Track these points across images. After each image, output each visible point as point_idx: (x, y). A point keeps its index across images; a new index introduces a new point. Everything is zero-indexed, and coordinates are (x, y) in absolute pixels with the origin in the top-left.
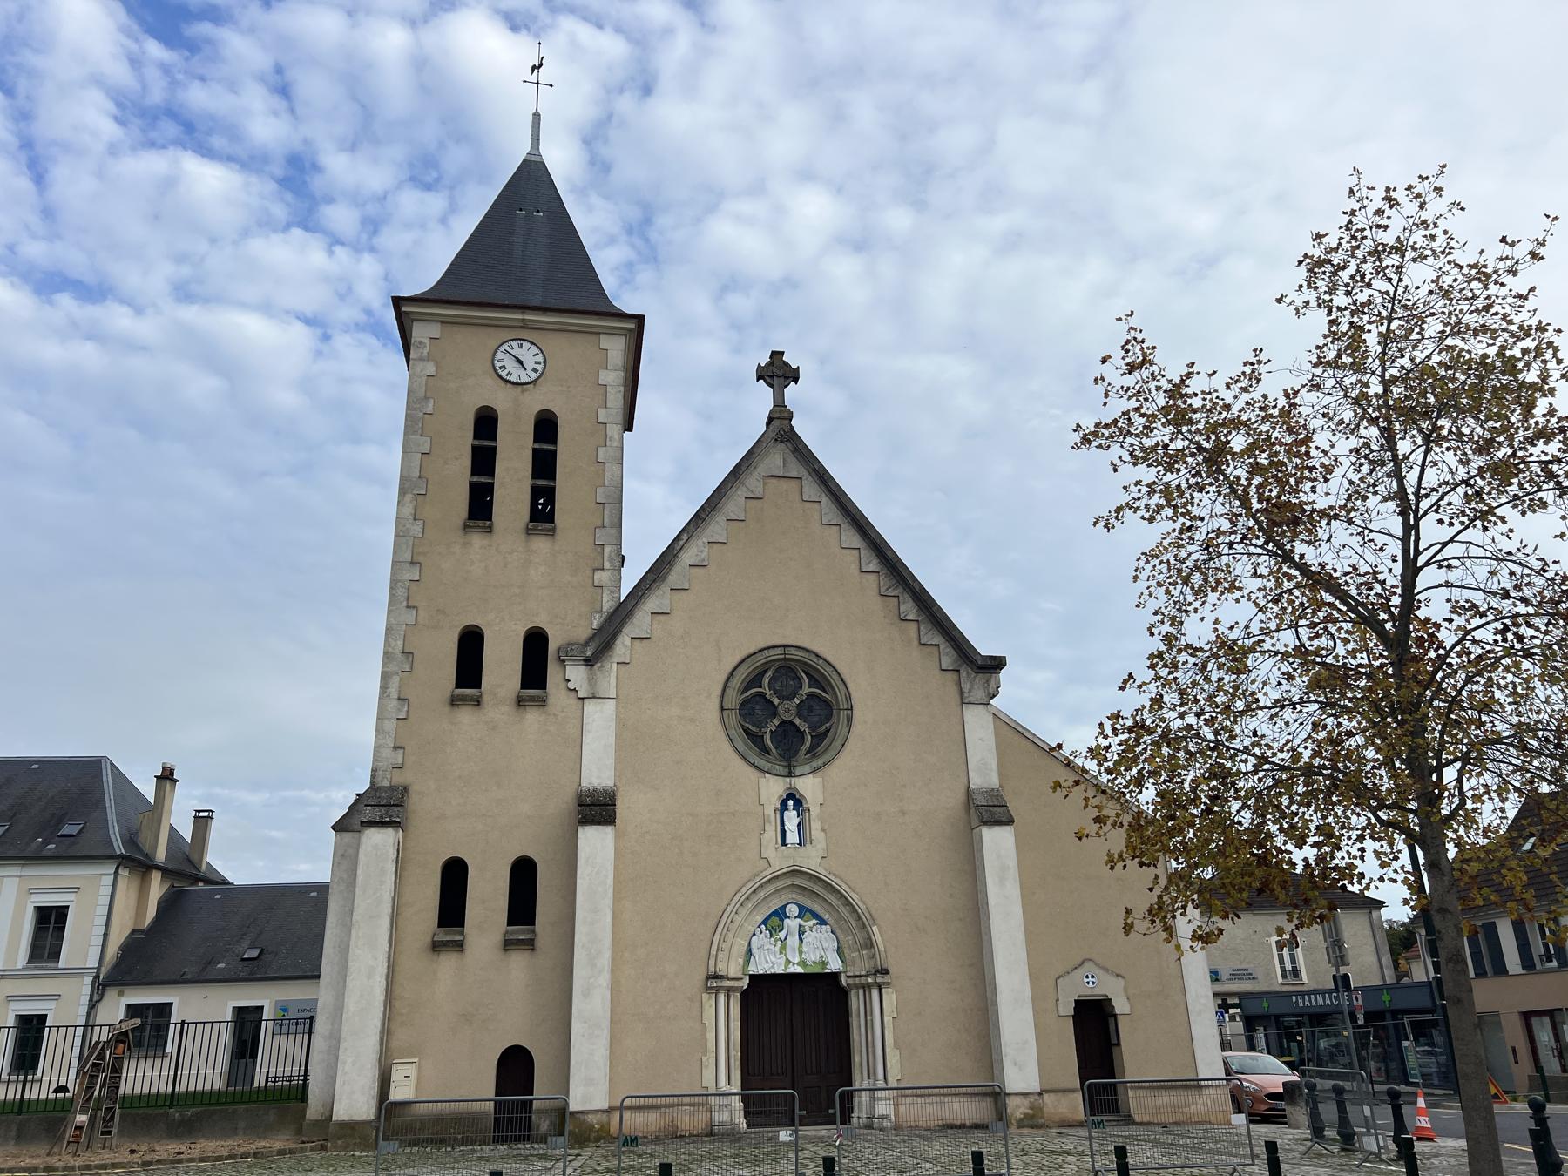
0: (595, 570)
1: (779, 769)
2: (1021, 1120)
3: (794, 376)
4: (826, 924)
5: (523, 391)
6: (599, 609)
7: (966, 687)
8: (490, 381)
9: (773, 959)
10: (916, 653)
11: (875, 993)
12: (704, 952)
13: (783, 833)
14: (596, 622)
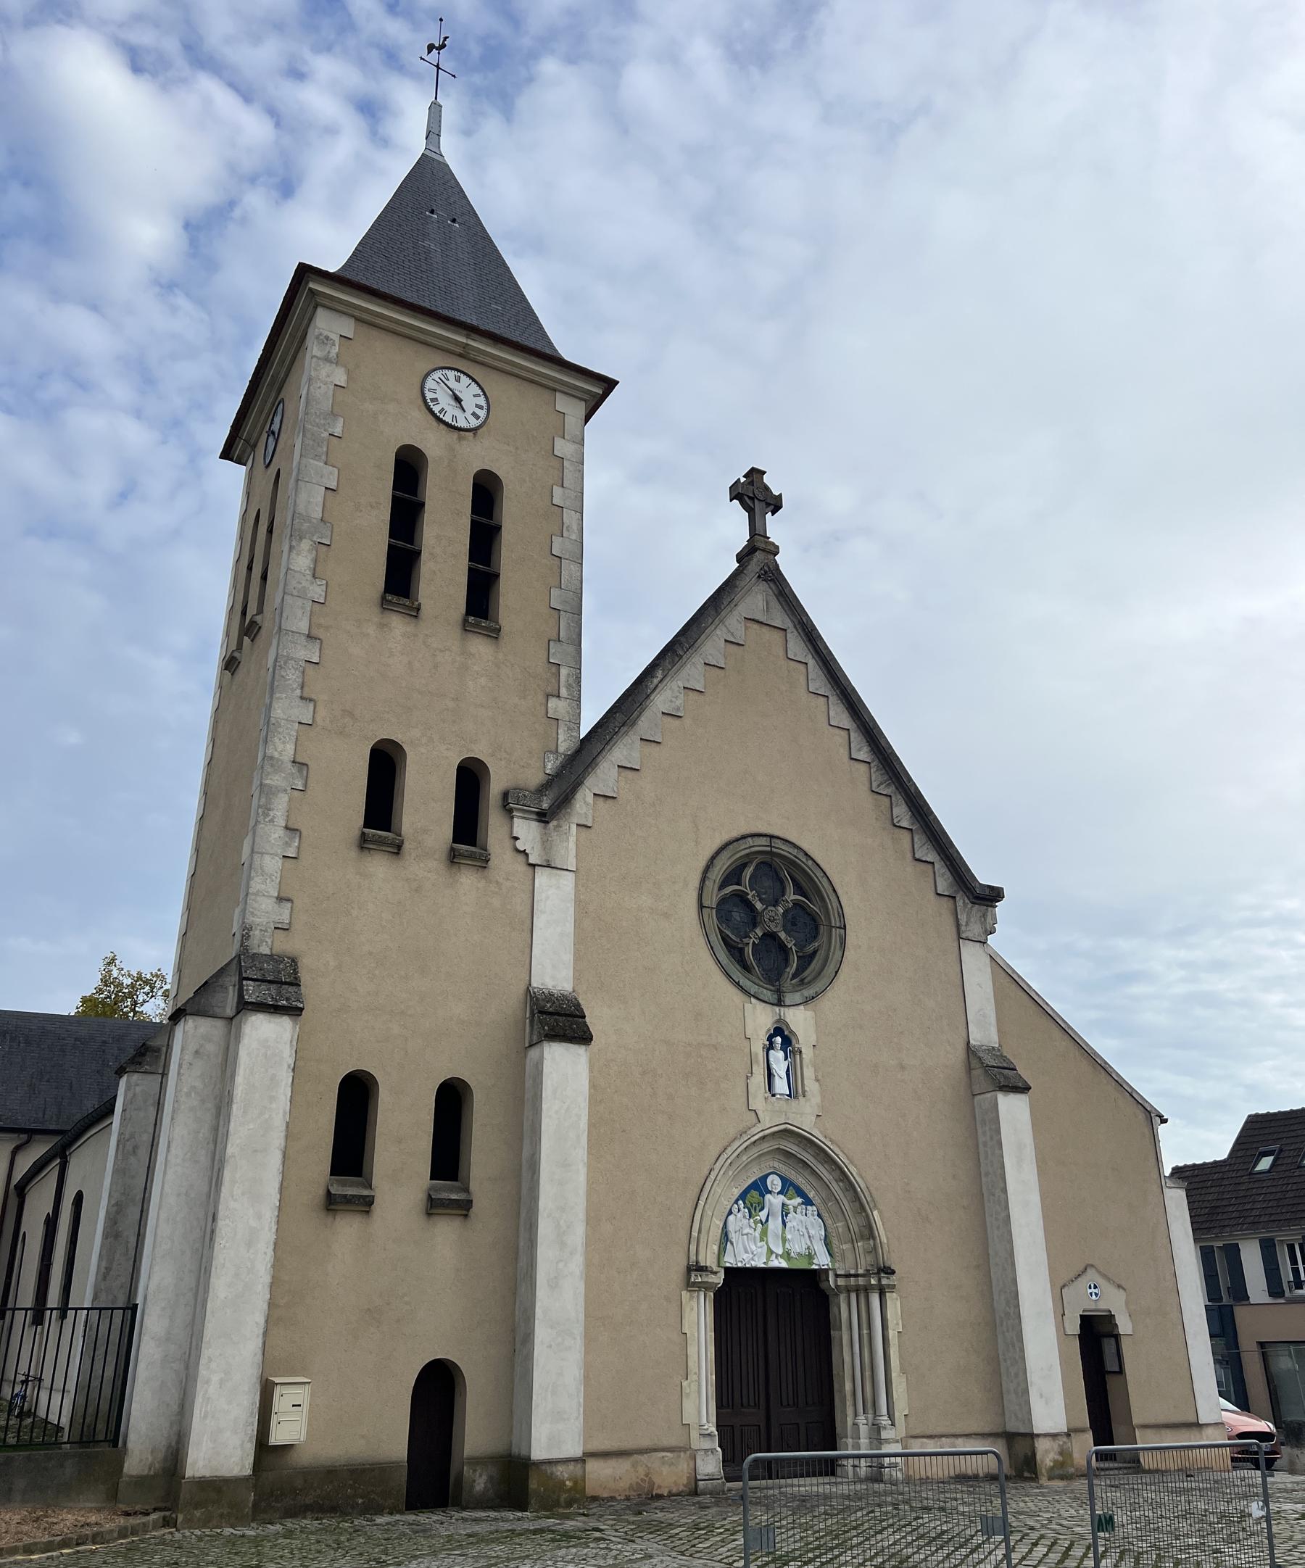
0: (548, 696)
1: (767, 995)
2: (1052, 1468)
3: (775, 505)
4: (812, 1204)
5: (460, 439)
6: (553, 749)
7: (963, 918)
8: (419, 414)
9: (754, 1248)
10: (910, 868)
11: (875, 1299)
12: (683, 1235)
13: (770, 1075)
14: (551, 765)
